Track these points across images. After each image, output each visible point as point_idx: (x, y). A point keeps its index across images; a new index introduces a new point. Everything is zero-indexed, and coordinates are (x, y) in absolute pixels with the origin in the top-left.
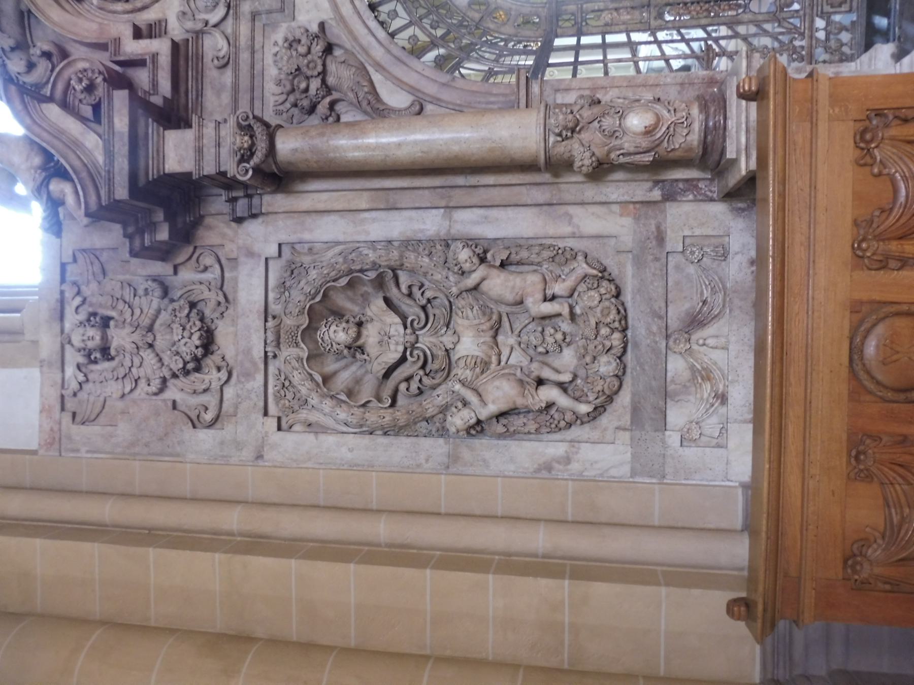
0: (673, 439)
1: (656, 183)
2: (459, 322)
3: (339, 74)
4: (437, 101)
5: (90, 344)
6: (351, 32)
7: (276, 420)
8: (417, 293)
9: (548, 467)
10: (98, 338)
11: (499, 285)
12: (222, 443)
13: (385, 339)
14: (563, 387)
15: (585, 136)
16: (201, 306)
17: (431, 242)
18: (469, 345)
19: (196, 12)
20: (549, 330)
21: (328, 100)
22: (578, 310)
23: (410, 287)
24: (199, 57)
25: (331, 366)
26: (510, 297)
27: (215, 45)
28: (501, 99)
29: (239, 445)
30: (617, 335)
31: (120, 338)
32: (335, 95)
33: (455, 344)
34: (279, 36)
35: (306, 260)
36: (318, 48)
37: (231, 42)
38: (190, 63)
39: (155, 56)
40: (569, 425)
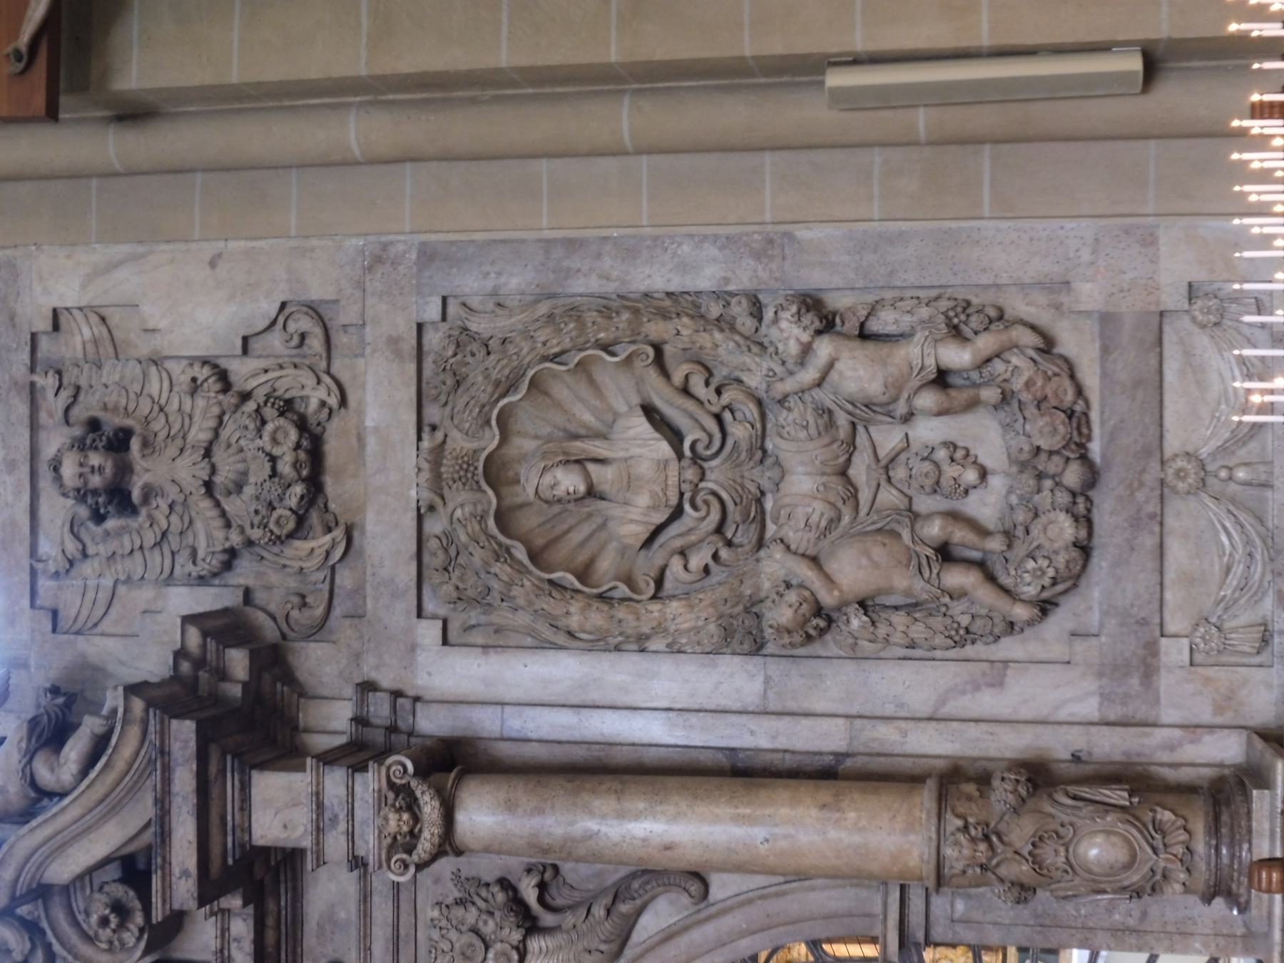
5: (96, 481)
7: (439, 624)
10: (109, 471)
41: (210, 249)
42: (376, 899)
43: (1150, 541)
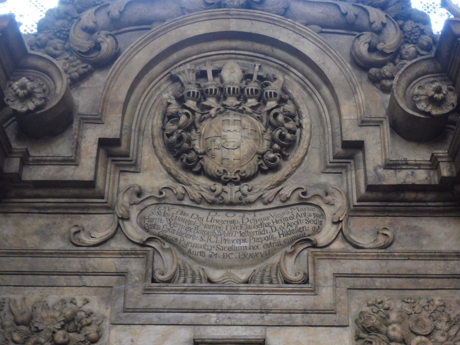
19: (141, 207)
24: (85, 210)
27: (98, 227)
34: (96, 306)
37: (97, 248)
38: (75, 200)
42: (442, 263)
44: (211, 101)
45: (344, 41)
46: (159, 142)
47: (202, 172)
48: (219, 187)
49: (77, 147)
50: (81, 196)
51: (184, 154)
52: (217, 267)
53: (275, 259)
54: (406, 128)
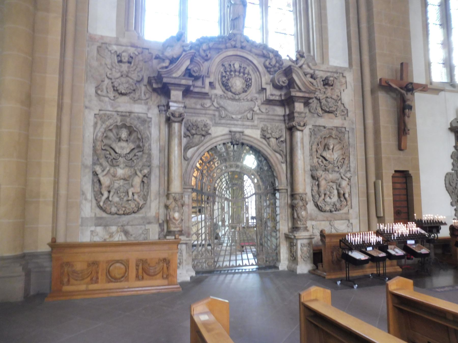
0: (93, 228)
1: (164, 222)
2: (127, 170)
3: (197, 138)
4: (188, 164)
6: (208, 142)
8: (136, 157)
9: (83, 194)
11: (137, 181)
12: (91, 96)
13: (122, 148)
14: (108, 198)
15: (174, 203)
16: (134, 92)
17: (150, 161)
18: (120, 172)
20: (124, 194)
21: (190, 135)
22: (130, 202)
23: (137, 155)
24: (205, 98)
25: (114, 131)
26: (134, 183)
27: (208, 103)
28: (188, 181)
29: (90, 101)
30: (122, 212)
31: (125, 67)
32: (191, 137)
33: (121, 168)
34: (208, 122)
35: (146, 126)
36: (204, 133)
39: (204, 88)
40: (96, 200)
41: (353, 100)
43: (325, 219)
44: (232, 73)
45: (263, 60)
46: (220, 82)
47: (231, 91)
48: (234, 96)
49: (203, 83)
50: (205, 95)
51: (226, 86)
52: (234, 114)
53: (246, 114)
54: (276, 87)
